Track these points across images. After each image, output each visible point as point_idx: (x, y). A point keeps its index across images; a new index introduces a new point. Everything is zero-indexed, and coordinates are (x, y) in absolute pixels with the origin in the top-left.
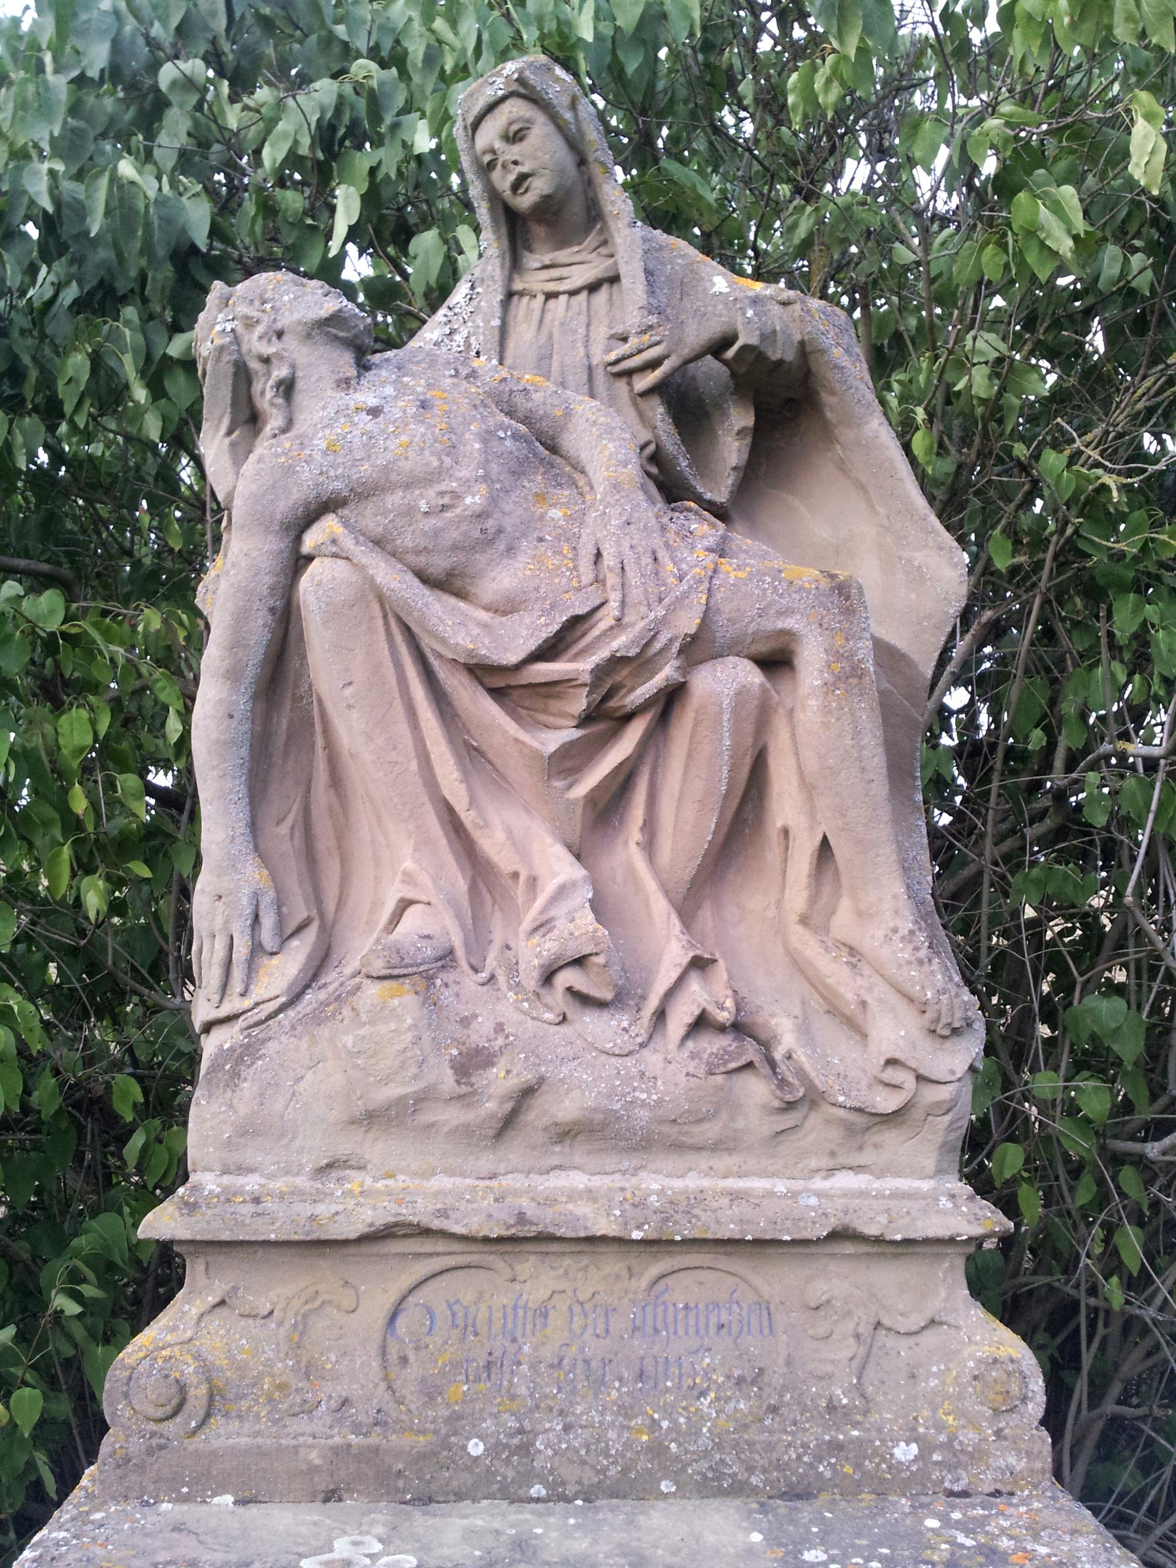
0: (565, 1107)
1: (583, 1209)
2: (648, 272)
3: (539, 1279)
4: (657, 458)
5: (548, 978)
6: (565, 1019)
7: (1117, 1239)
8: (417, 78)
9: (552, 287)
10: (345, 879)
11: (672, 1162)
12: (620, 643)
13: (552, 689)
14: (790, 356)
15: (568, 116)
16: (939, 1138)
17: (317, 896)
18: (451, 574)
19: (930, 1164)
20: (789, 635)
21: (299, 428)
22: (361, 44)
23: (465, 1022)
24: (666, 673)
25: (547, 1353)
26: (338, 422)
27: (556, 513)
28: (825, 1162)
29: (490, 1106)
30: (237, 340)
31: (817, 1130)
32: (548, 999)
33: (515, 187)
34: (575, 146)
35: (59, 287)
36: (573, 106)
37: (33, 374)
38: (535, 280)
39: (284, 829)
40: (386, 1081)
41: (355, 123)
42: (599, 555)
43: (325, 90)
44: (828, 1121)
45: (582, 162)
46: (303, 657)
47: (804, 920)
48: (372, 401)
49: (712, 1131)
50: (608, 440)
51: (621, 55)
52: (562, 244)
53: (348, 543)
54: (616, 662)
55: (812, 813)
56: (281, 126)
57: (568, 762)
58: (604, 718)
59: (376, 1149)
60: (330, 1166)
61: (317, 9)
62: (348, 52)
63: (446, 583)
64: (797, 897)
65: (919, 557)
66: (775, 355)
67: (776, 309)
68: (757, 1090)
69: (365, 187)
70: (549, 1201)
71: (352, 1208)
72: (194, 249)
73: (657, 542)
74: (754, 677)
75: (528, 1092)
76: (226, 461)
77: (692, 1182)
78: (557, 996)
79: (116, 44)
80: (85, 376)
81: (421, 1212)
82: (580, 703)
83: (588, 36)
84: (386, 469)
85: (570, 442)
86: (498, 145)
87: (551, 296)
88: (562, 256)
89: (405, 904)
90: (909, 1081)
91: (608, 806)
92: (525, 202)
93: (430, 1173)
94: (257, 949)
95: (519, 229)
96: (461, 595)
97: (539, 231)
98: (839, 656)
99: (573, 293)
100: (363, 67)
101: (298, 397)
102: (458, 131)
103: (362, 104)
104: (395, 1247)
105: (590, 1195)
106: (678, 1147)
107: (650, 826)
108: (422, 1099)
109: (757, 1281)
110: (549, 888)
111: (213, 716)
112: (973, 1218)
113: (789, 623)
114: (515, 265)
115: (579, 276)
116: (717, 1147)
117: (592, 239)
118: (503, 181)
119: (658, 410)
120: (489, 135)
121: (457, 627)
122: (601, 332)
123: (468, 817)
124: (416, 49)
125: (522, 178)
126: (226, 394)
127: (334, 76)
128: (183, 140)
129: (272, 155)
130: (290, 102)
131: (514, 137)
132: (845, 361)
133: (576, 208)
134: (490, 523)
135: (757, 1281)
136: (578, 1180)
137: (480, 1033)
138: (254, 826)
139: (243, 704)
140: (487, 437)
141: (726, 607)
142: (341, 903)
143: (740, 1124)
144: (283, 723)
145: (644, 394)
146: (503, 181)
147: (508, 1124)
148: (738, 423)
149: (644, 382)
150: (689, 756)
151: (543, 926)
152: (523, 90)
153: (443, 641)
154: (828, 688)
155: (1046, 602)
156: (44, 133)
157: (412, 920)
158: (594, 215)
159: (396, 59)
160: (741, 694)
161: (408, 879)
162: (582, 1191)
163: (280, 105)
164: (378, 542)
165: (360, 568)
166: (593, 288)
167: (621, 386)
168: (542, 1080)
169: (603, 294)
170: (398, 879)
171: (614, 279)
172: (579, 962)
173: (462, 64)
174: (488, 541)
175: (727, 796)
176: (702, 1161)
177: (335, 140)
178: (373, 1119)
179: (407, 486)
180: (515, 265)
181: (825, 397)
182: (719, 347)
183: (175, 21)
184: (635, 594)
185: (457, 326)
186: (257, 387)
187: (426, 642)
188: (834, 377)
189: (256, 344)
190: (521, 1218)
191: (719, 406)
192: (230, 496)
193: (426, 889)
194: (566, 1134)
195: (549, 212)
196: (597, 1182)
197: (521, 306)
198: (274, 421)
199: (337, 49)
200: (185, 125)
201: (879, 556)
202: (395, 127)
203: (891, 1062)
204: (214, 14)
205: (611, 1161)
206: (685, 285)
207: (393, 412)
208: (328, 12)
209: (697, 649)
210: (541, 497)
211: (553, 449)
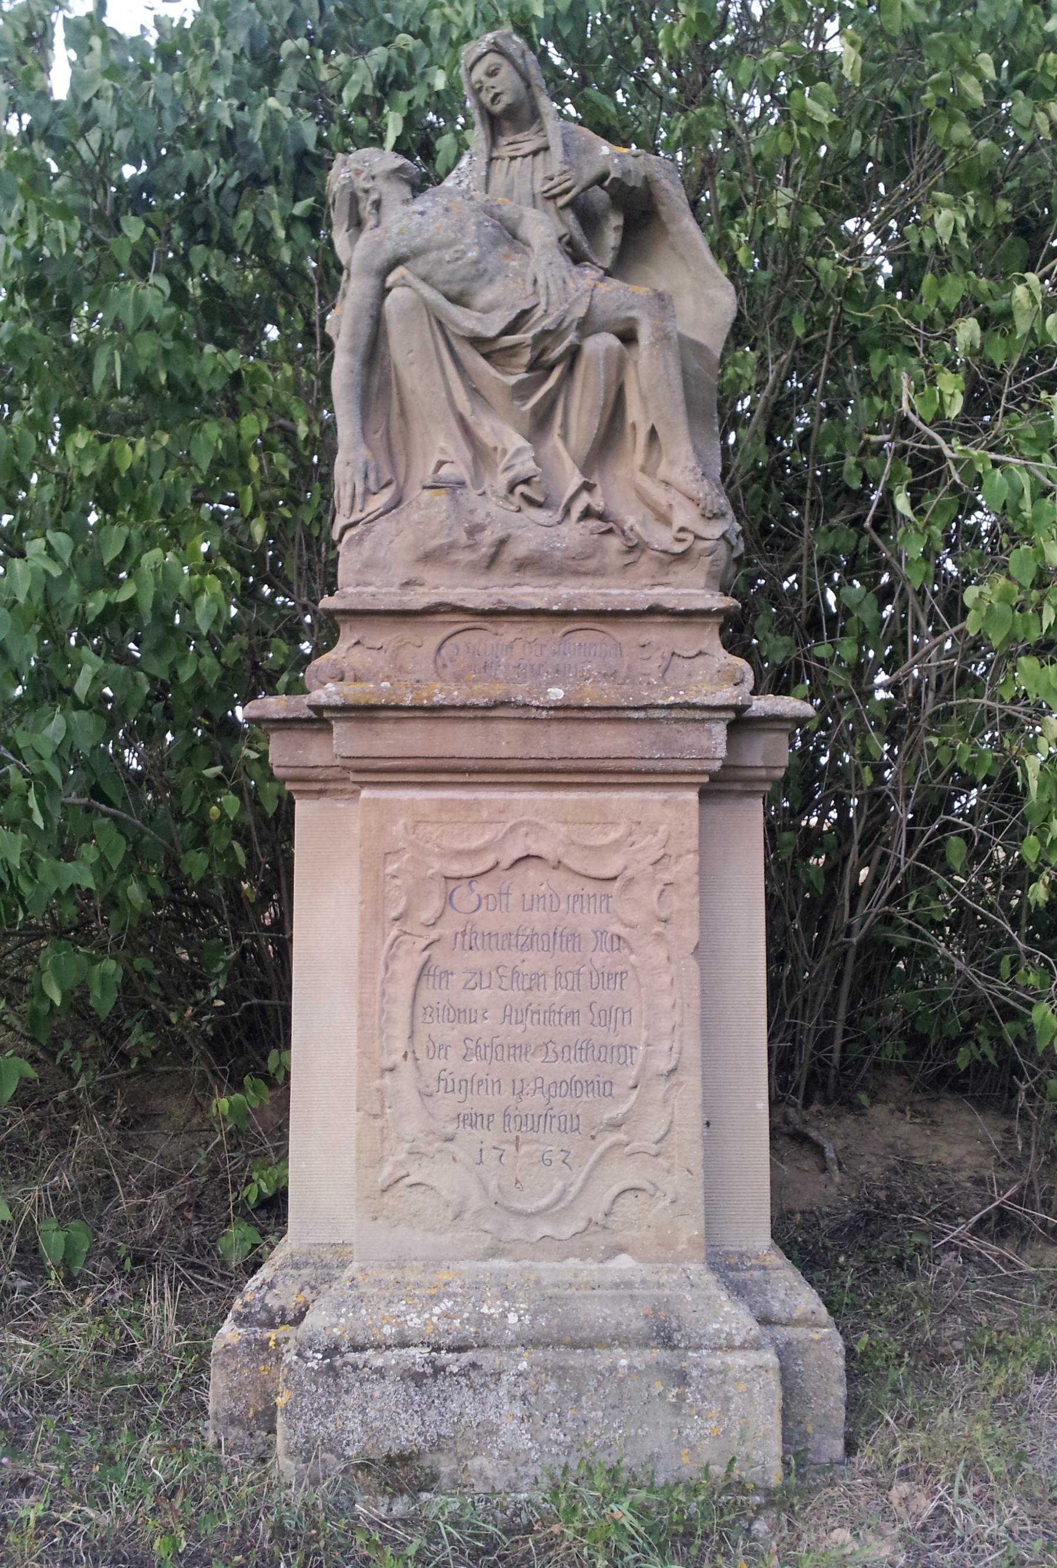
0: (519, 550)
2: (565, 145)
3: (509, 632)
4: (570, 243)
5: (511, 489)
6: (519, 510)
7: (868, 742)
8: (435, 45)
10: (408, 466)
11: (573, 581)
12: (547, 323)
13: (512, 350)
14: (639, 184)
15: (520, 61)
16: (706, 568)
17: (394, 470)
18: (462, 294)
19: (702, 581)
20: (633, 321)
21: (383, 225)
22: (400, 25)
23: (472, 512)
24: (571, 338)
25: (513, 663)
26: (403, 219)
27: (514, 263)
28: (650, 581)
29: (484, 550)
30: (352, 182)
31: (645, 564)
32: (512, 498)
33: (493, 100)
34: (525, 77)
35: (227, 177)
36: (523, 55)
37: (218, 225)
38: (504, 151)
39: (378, 436)
40: (434, 537)
41: (398, 74)
42: (535, 281)
43: (379, 54)
44: (652, 559)
45: (528, 86)
46: (387, 345)
47: (643, 469)
48: (420, 209)
49: (592, 564)
50: (542, 228)
51: (560, 26)
52: (519, 130)
53: (410, 277)
54: (546, 333)
55: (646, 412)
56: (354, 77)
57: (522, 391)
58: (539, 367)
60: (407, 584)
61: (372, 4)
62: (393, 30)
63: (459, 300)
64: (639, 458)
65: (712, 292)
66: (631, 183)
67: (631, 159)
68: (615, 543)
69: (405, 113)
71: (417, 599)
72: (306, 152)
73: (565, 274)
74: (616, 343)
75: (502, 543)
76: (347, 244)
77: (583, 590)
78: (516, 499)
79: (252, 33)
80: (250, 224)
82: (526, 357)
83: (540, 14)
84: (429, 240)
85: (522, 232)
86: (484, 78)
87: (513, 158)
88: (519, 137)
89: (441, 464)
90: (690, 537)
92: (498, 108)
94: (367, 492)
95: (498, 123)
96: (466, 305)
97: (506, 124)
98: (658, 329)
99: (524, 156)
100: (403, 39)
101: (384, 210)
102: (462, 71)
103: (403, 63)
104: (440, 618)
105: (533, 594)
106: (576, 573)
107: (565, 425)
108: (452, 546)
110: (511, 451)
113: (633, 313)
114: (493, 144)
115: (528, 147)
116: (595, 573)
117: (535, 128)
118: (486, 97)
119: (570, 217)
120: (479, 73)
121: (466, 320)
122: (539, 176)
123: (470, 419)
124: (435, 27)
125: (497, 95)
126: (346, 210)
127: (385, 45)
128: (293, 89)
129: (349, 95)
130: (361, 62)
131: (492, 73)
132: (669, 187)
133: (525, 112)
134: (481, 266)
137: (479, 517)
138: (363, 428)
139: (357, 366)
140: (479, 224)
141: (601, 305)
142: (406, 478)
143: (607, 560)
144: (376, 381)
145: (563, 208)
146: (486, 97)
147: (492, 561)
149: (562, 201)
150: (584, 386)
151: (507, 469)
152: (496, 49)
153: (457, 325)
154: (652, 345)
155: (831, 361)
156: (220, 85)
157: (445, 470)
158: (535, 115)
159: (423, 34)
160: (609, 350)
161: (443, 451)
162: (532, 593)
163: (352, 65)
164: (425, 279)
165: (416, 290)
166: (535, 153)
167: (550, 205)
168: (509, 536)
169: (540, 157)
170: (438, 449)
171: (546, 149)
172: (527, 481)
173: (147, 543)
174: (480, 275)
175: (604, 407)
176: (589, 581)
177: (389, 84)
178: (429, 558)
179: (439, 248)
180: (493, 144)
181: (661, 208)
182: (600, 179)
183: (287, 16)
184: (554, 298)
185: (465, 175)
186: (361, 206)
187: (450, 328)
188: (663, 195)
189: (361, 183)
190: (500, 602)
191: (605, 217)
192: (349, 263)
193: (452, 454)
194: (522, 565)
195: (510, 112)
196: (538, 590)
197: (497, 165)
198: (371, 222)
199: (385, 30)
200: (295, 80)
201: (695, 294)
202: (423, 75)
203: (682, 529)
204: (311, 10)
205: (543, 581)
206: (587, 149)
207: (432, 213)
208: (380, 5)
209: (586, 326)
210: (507, 256)
211: (515, 236)
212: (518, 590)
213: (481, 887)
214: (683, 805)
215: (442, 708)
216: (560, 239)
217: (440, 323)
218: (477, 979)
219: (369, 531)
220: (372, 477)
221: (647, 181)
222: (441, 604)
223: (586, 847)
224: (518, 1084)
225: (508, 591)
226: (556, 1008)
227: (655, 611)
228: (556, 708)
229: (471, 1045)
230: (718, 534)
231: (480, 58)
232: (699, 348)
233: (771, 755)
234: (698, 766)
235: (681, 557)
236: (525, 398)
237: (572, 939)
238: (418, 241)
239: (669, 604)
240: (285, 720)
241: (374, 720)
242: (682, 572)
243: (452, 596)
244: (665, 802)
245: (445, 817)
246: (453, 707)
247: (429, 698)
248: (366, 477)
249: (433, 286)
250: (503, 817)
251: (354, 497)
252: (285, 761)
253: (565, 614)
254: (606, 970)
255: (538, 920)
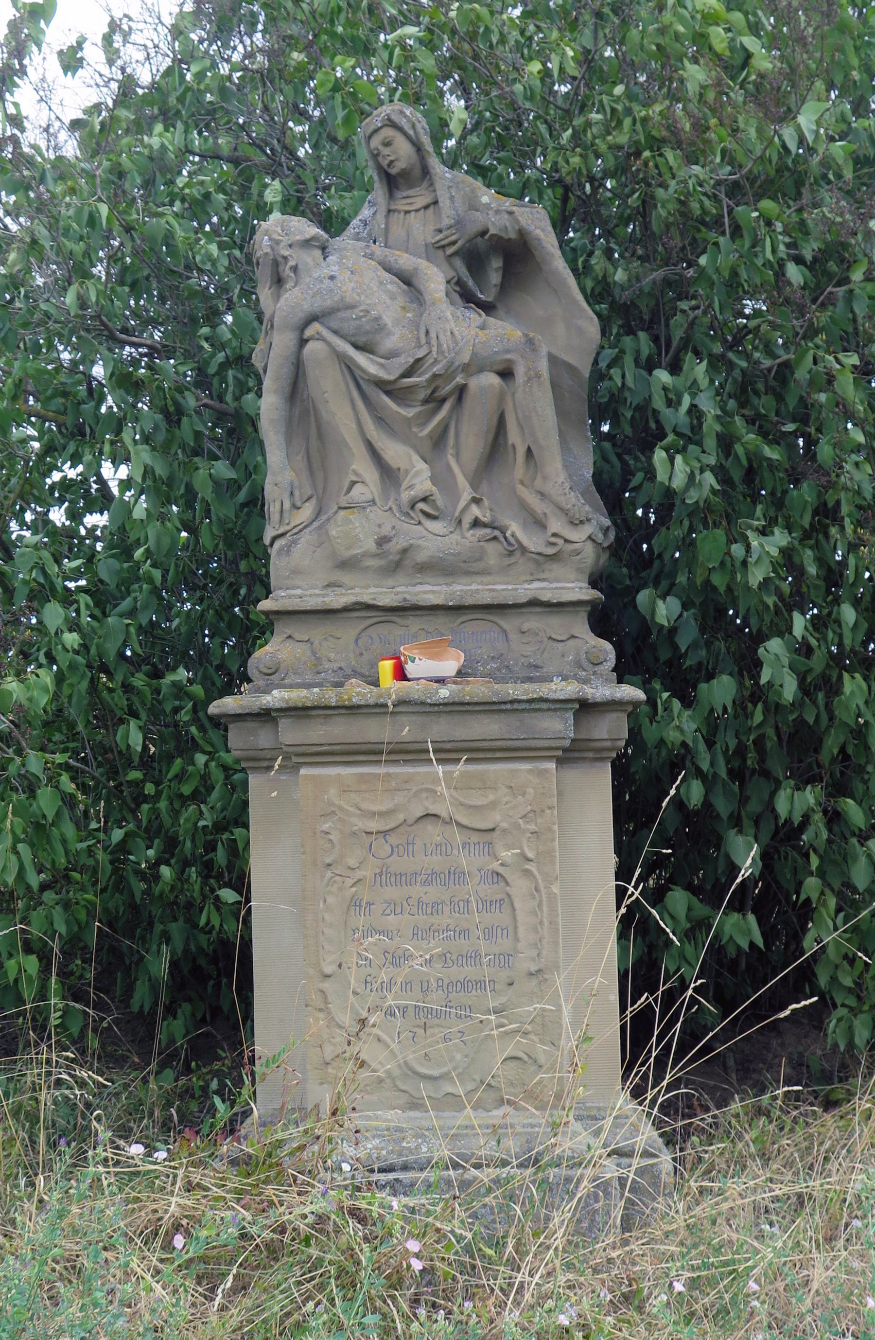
0: (422, 557)
1: (431, 596)
4: (459, 283)
9: (407, 208)
10: (326, 479)
11: (464, 580)
13: (410, 388)
15: (411, 132)
20: (510, 361)
28: (529, 578)
39: (299, 458)
42: (427, 332)
46: (305, 382)
49: (480, 566)
50: (435, 280)
54: (435, 376)
59: (346, 578)
70: (416, 594)
71: (337, 600)
75: (405, 551)
77: (474, 587)
81: (366, 598)
87: (407, 212)
88: (411, 192)
89: (354, 483)
91: (439, 440)
93: (367, 587)
99: (417, 211)
105: (433, 592)
106: (468, 573)
107: (457, 446)
109: (502, 623)
111: (269, 406)
112: (588, 594)
113: (509, 356)
115: (420, 202)
117: (425, 184)
119: (458, 262)
120: (375, 142)
135: (502, 623)
136: (428, 588)
148: (493, 268)
149: (450, 250)
162: (432, 592)
166: (426, 207)
167: (440, 253)
171: (436, 203)
172: (424, 500)
176: (479, 579)
180: (391, 195)
187: (357, 373)
190: (405, 600)
192: (272, 316)
196: (435, 588)
201: (561, 327)
203: (555, 535)
205: (441, 580)
212: (419, 588)
213: (393, 839)
214: (542, 773)
215: (359, 707)
216: (448, 282)
217: (349, 368)
218: (394, 907)
219: (295, 542)
220: (297, 493)
221: (522, 233)
222: (357, 603)
223: (471, 807)
224: (425, 985)
225: (410, 588)
226: (451, 927)
227: (534, 603)
228: (445, 704)
229: (389, 956)
230: (584, 537)
231: (376, 131)
232: (571, 369)
233: (612, 730)
234: (557, 743)
235: (554, 558)
236: (424, 424)
237: (456, 875)
238: (328, 303)
239: (546, 597)
240: (240, 715)
241: (309, 717)
242: (556, 569)
243: (366, 597)
244: (530, 771)
245: (364, 787)
246: (367, 706)
247: (350, 699)
248: (292, 493)
249: (343, 337)
250: (408, 786)
251: (282, 511)
252: (241, 745)
253: (458, 609)
254: (488, 899)
255: (435, 862)
